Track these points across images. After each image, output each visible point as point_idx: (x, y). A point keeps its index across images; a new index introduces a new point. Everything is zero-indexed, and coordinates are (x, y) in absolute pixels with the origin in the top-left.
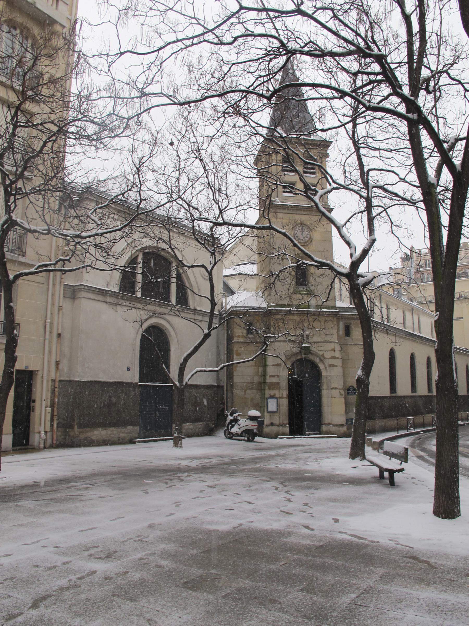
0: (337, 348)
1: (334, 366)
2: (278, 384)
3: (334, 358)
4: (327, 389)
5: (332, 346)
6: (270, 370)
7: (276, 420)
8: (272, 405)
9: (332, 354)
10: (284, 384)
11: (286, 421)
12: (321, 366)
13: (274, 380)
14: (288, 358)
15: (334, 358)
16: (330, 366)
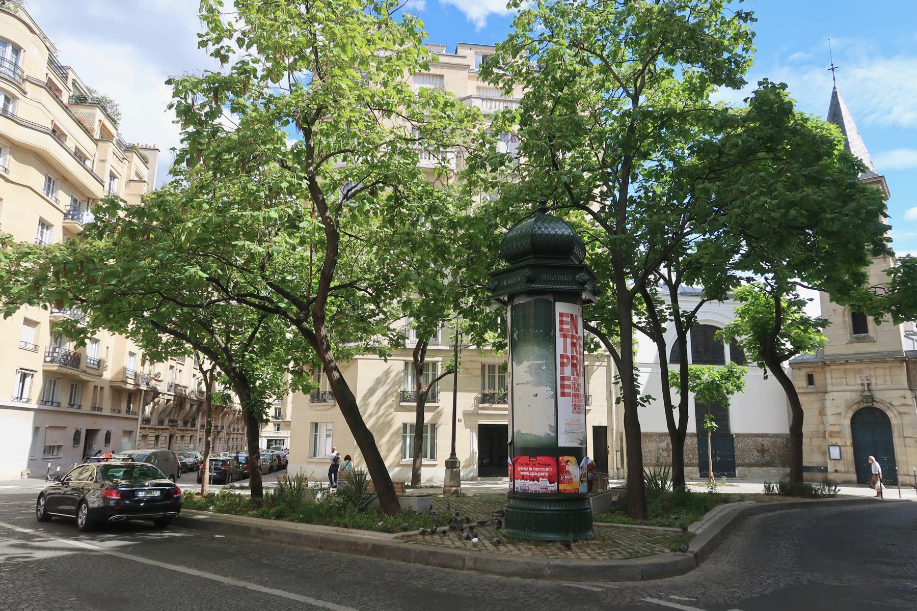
0: (909, 394)
1: (905, 413)
2: (840, 432)
3: (906, 405)
4: (900, 437)
5: (901, 393)
6: (830, 419)
7: (840, 467)
8: (835, 452)
9: (903, 401)
10: (848, 432)
11: (852, 469)
12: (890, 414)
13: (836, 428)
14: (849, 407)
15: (906, 405)
16: (900, 413)
